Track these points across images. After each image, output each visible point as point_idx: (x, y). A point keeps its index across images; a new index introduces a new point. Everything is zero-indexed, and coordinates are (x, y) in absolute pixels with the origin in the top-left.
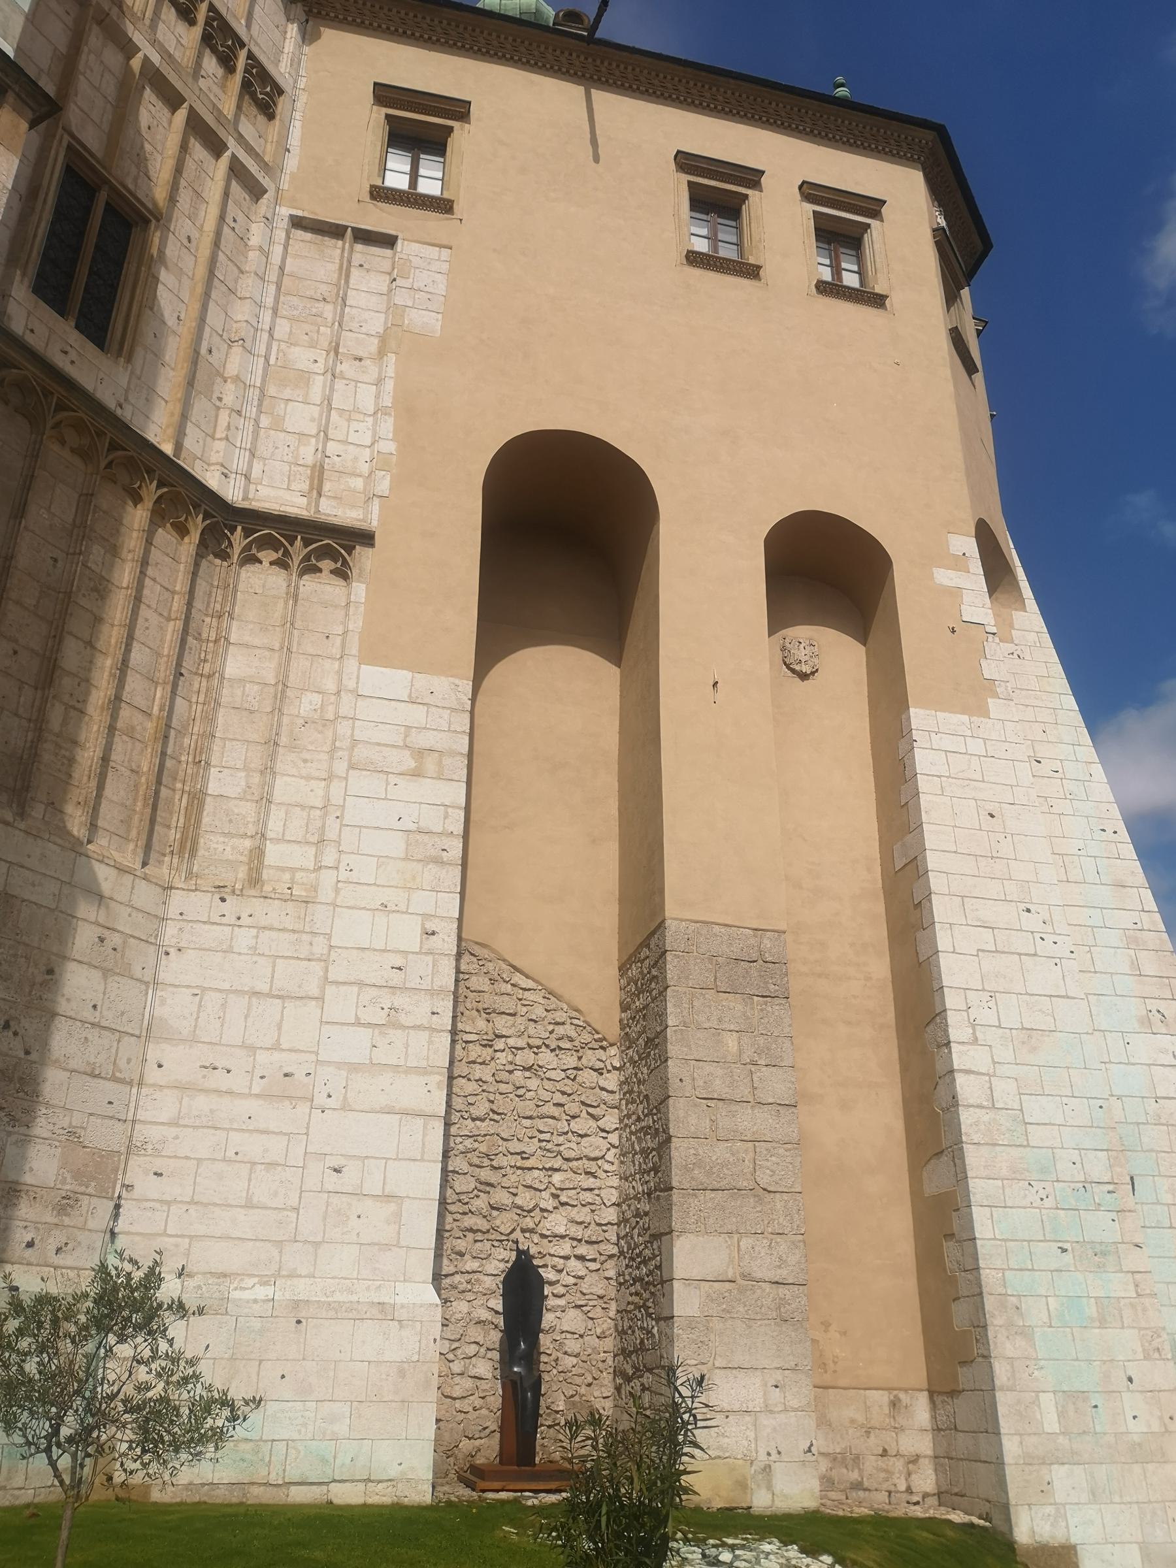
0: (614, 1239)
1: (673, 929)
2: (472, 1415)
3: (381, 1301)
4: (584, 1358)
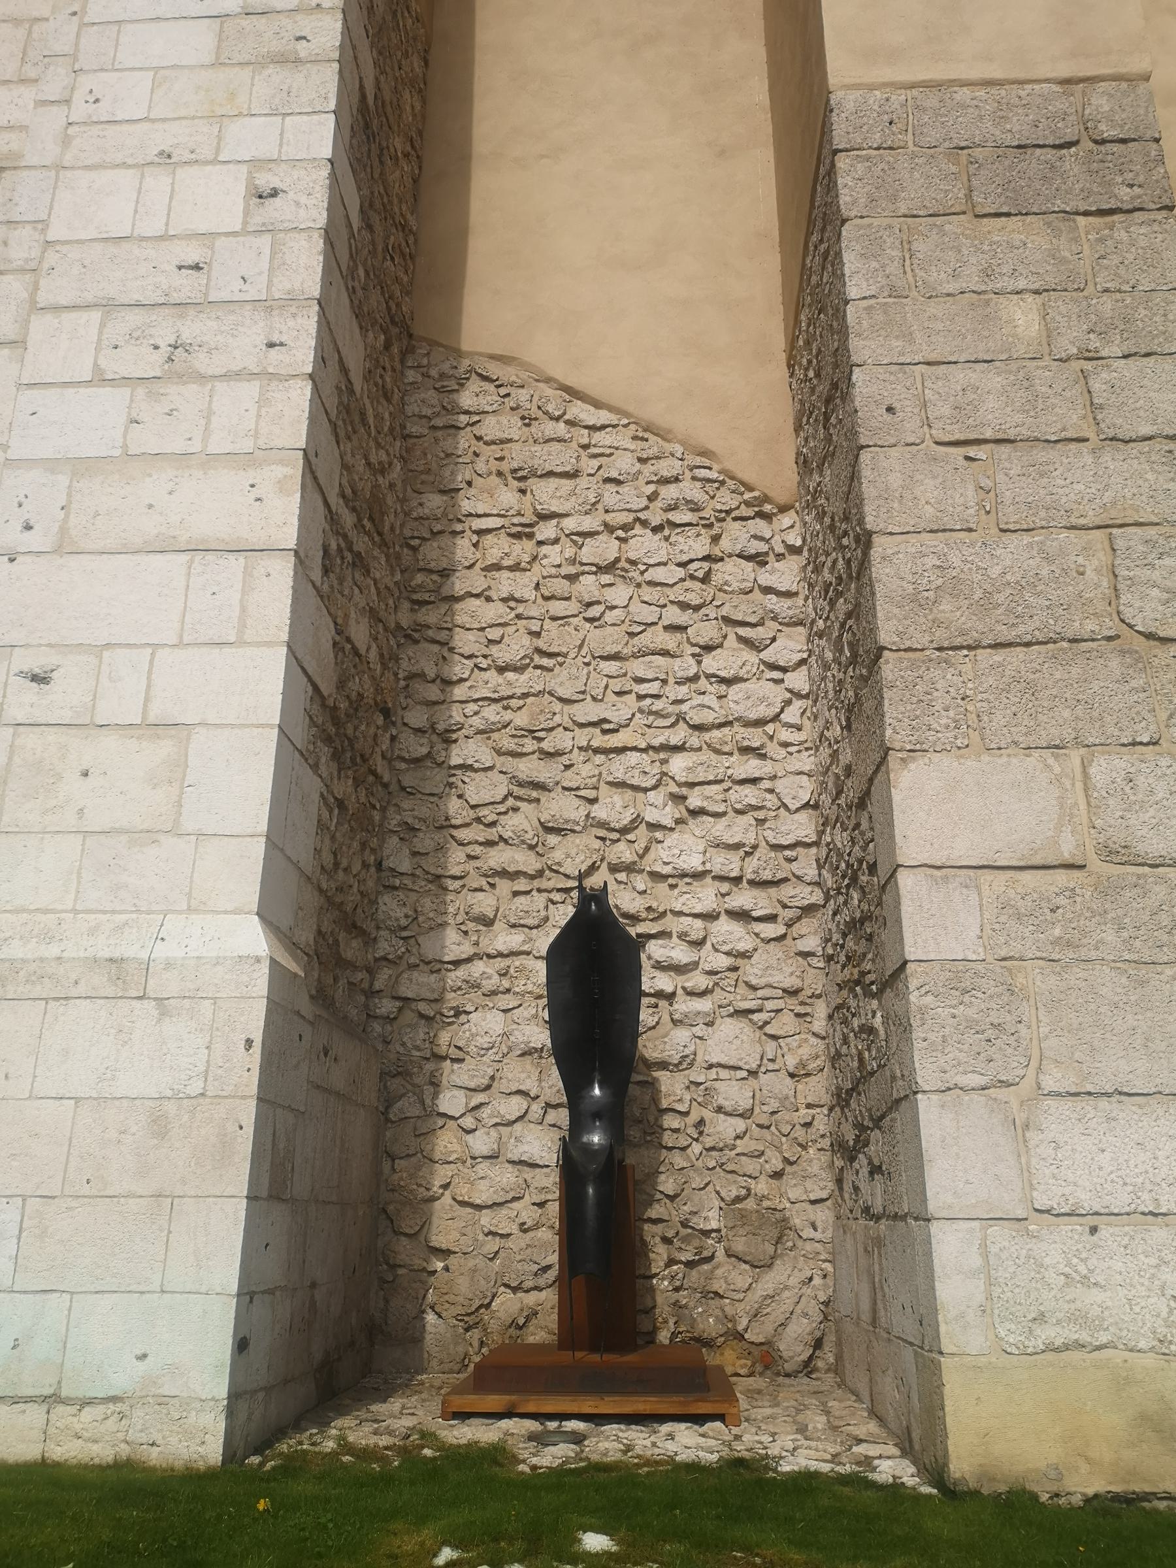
0: (811, 873)
1: (850, 106)
2: (518, 1242)
3: (117, 955)
4: (764, 1120)
